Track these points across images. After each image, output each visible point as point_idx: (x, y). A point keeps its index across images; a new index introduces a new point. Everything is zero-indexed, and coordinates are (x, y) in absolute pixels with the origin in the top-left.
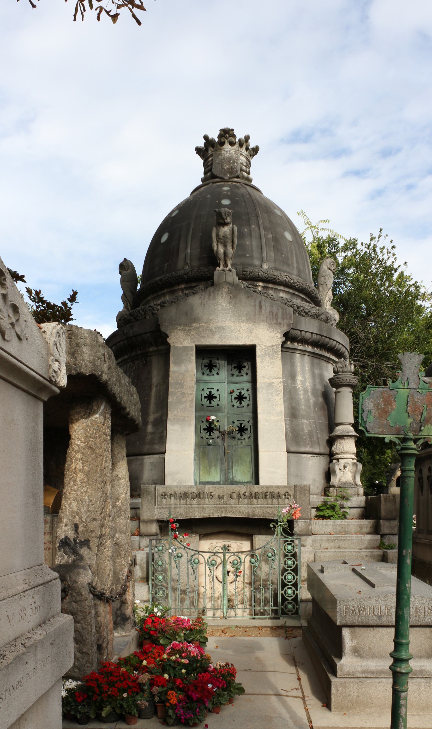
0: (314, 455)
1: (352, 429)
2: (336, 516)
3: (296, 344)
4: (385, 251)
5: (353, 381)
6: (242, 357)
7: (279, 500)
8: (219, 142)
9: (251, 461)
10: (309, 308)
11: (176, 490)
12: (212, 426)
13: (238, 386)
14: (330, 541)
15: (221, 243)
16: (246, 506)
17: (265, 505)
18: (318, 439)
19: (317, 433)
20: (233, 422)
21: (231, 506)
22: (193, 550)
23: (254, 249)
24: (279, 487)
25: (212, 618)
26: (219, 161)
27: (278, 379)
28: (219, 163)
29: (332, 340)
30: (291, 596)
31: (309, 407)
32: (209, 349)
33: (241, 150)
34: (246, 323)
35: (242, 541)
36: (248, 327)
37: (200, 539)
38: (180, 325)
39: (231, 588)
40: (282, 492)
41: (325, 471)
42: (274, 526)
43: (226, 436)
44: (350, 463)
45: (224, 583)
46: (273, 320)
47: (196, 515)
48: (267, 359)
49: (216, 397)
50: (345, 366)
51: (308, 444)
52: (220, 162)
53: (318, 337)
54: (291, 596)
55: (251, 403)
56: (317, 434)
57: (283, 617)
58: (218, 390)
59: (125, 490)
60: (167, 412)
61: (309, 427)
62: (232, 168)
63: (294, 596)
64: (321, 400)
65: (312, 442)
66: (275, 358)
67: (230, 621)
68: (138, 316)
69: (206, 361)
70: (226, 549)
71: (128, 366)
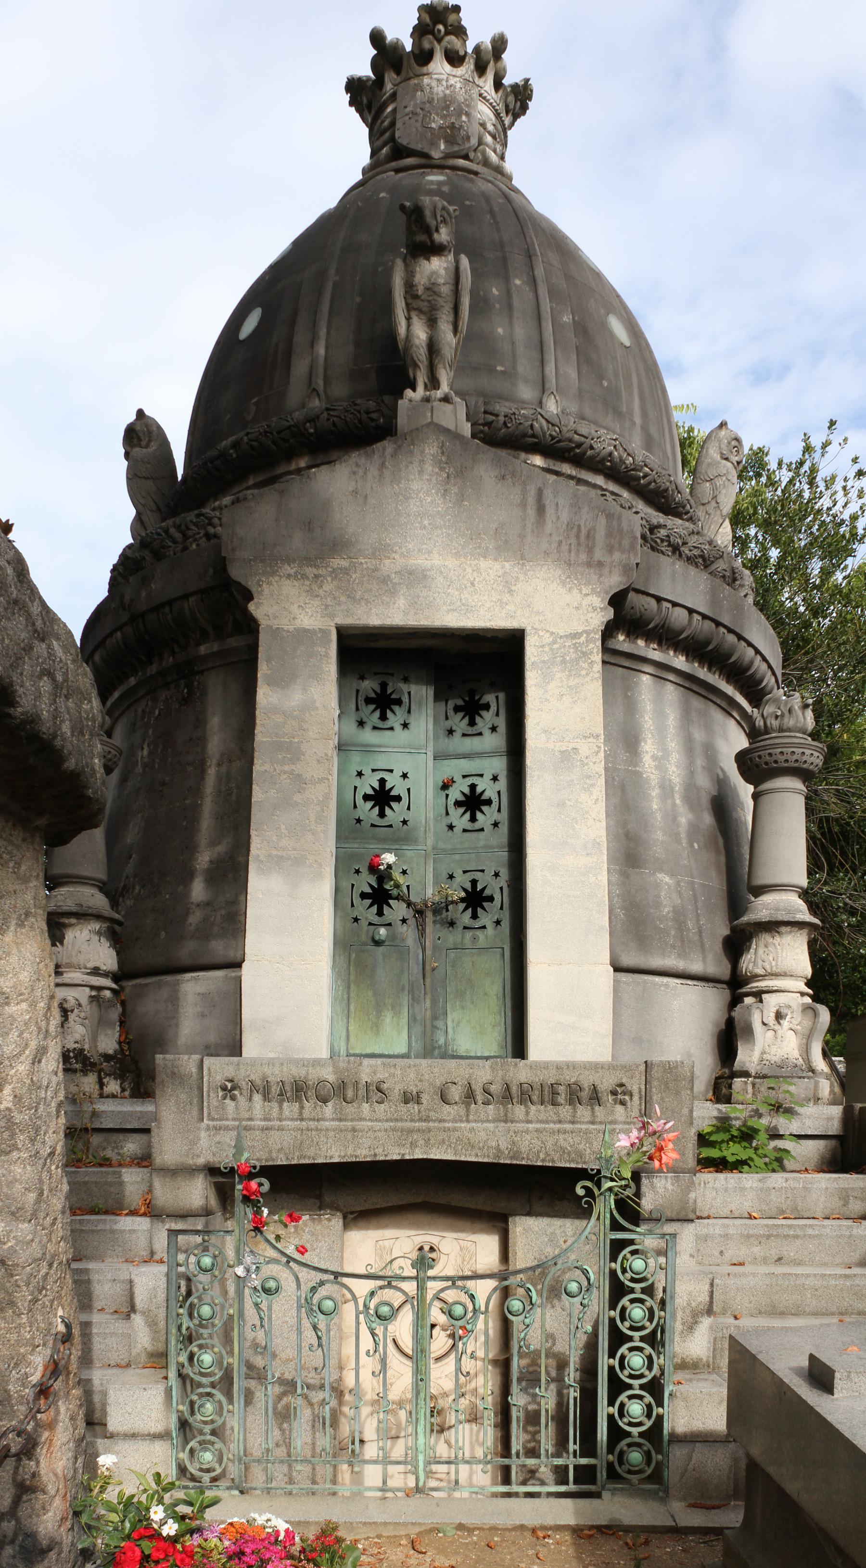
0: (695, 983)
1: (801, 904)
2: (758, 1161)
3: (641, 643)
4: (838, 486)
5: (812, 759)
6: (480, 672)
7: (597, 1108)
8: (417, 52)
9: (501, 995)
10: (683, 532)
11: (268, 1071)
12: (387, 887)
13: (467, 766)
14: (752, 1240)
15: (420, 311)
16: (490, 1126)
17: (552, 1125)
18: (700, 933)
19: (698, 915)
20: (451, 877)
21: (442, 1125)
22: (316, 1269)
23: (521, 350)
24: (596, 1067)
25: (379, 1494)
26: (415, 105)
27: (591, 740)
28: (415, 114)
29: (743, 643)
30: (640, 1424)
31: (678, 841)
32: (381, 644)
33: (480, 82)
34: (496, 560)
35: (474, 1233)
36: (500, 573)
37: (346, 1226)
38: (289, 560)
39: (442, 1377)
40: (606, 1083)
41: (717, 1030)
42: (589, 1192)
43: (429, 917)
44: (794, 1005)
45: (418, 1358)
46: (579, 551)
47: (333, 1152)
48: (559, 675)
49: (398, 799)
50: (790, 711)
51: (673, 947)
52: (419, 110)
53: (708, 625)
54: (640, 1424)
55: (504, 817)
56: (698, 920)
57: (613, 1492)
58: (405, 776)
59: (33, 1044)
60: (249, 837)
61: (675, 896)
62: (452, 126)
63: (649, 1424)
64: (708, 819)
65: (683, 941)
66: (583, 672)
67: (438, 1503)
68: (163, 547)
69: (369, 686)
70: (424, 1260)
71: (140, 710)
